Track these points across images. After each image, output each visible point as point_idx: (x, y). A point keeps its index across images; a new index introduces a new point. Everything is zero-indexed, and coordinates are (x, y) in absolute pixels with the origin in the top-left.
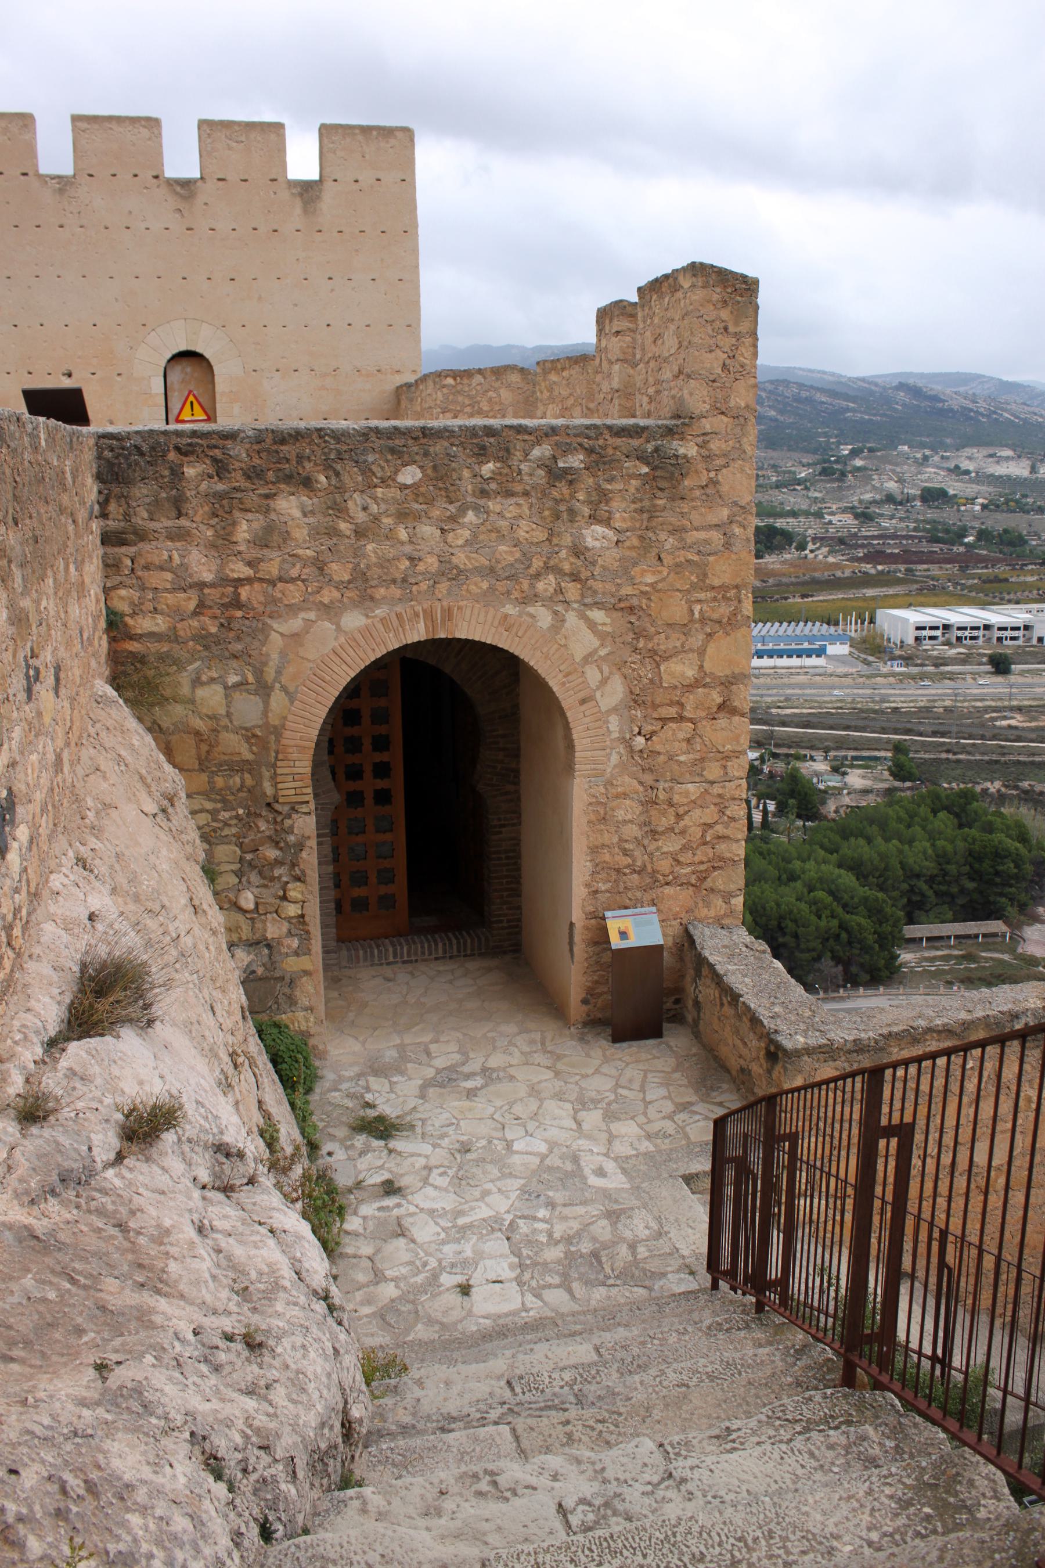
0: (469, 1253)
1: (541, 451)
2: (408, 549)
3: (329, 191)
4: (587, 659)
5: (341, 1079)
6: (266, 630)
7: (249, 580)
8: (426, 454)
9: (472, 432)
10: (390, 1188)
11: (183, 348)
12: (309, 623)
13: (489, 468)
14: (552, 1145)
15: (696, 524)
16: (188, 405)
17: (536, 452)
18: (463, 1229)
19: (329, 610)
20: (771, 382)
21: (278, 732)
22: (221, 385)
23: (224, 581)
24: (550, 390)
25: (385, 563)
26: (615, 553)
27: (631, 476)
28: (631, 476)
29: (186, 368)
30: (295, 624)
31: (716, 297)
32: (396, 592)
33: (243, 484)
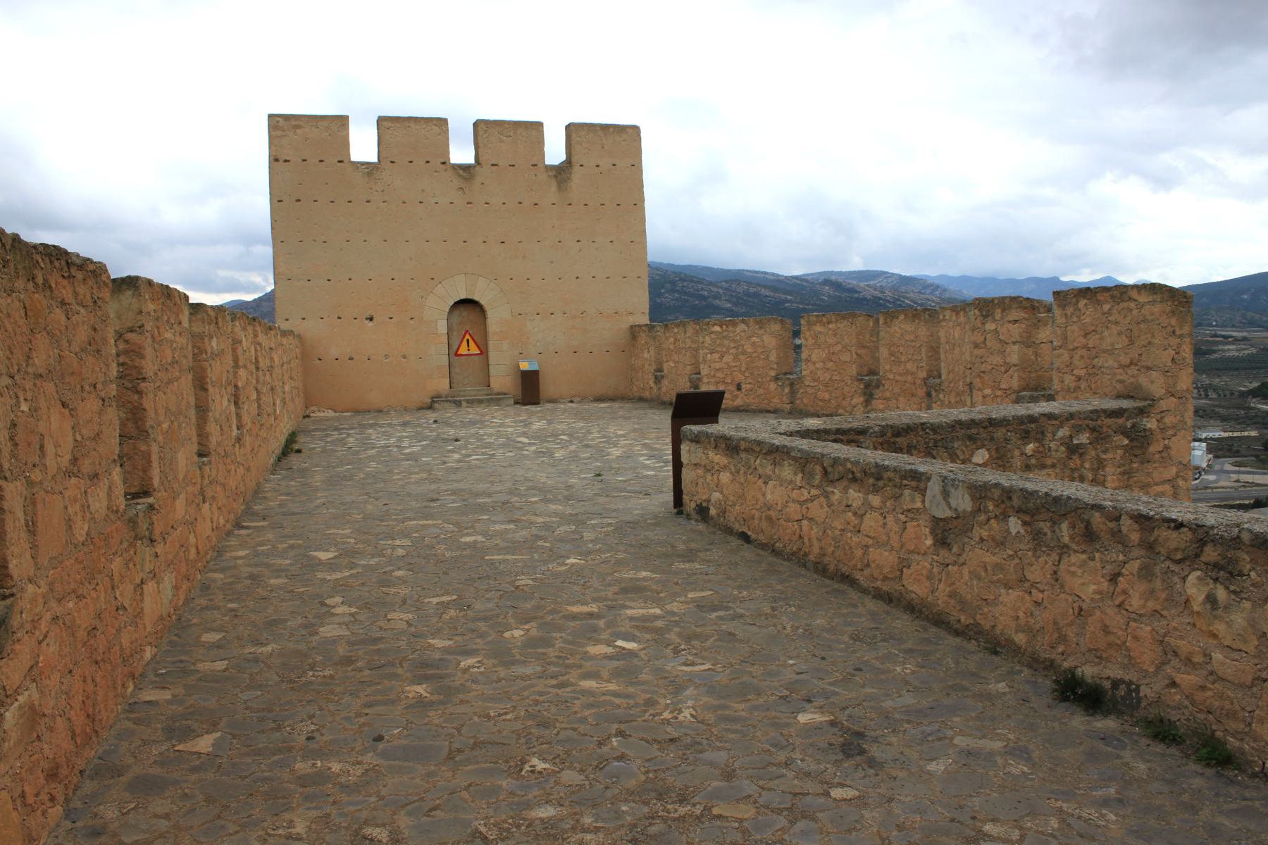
1: (1063, 432)
3: (577, 174)
8: (992, 439)
9: (1021, 420)
11: (463, 297)
13: (1030, 447)
15: (1156, 480)
16: (465, 342)
20: (726, 282)
24: (815, 337)
27: (1118, 447)
28: (1118, 447)
29: (465, 312)
31: (1168, 309)
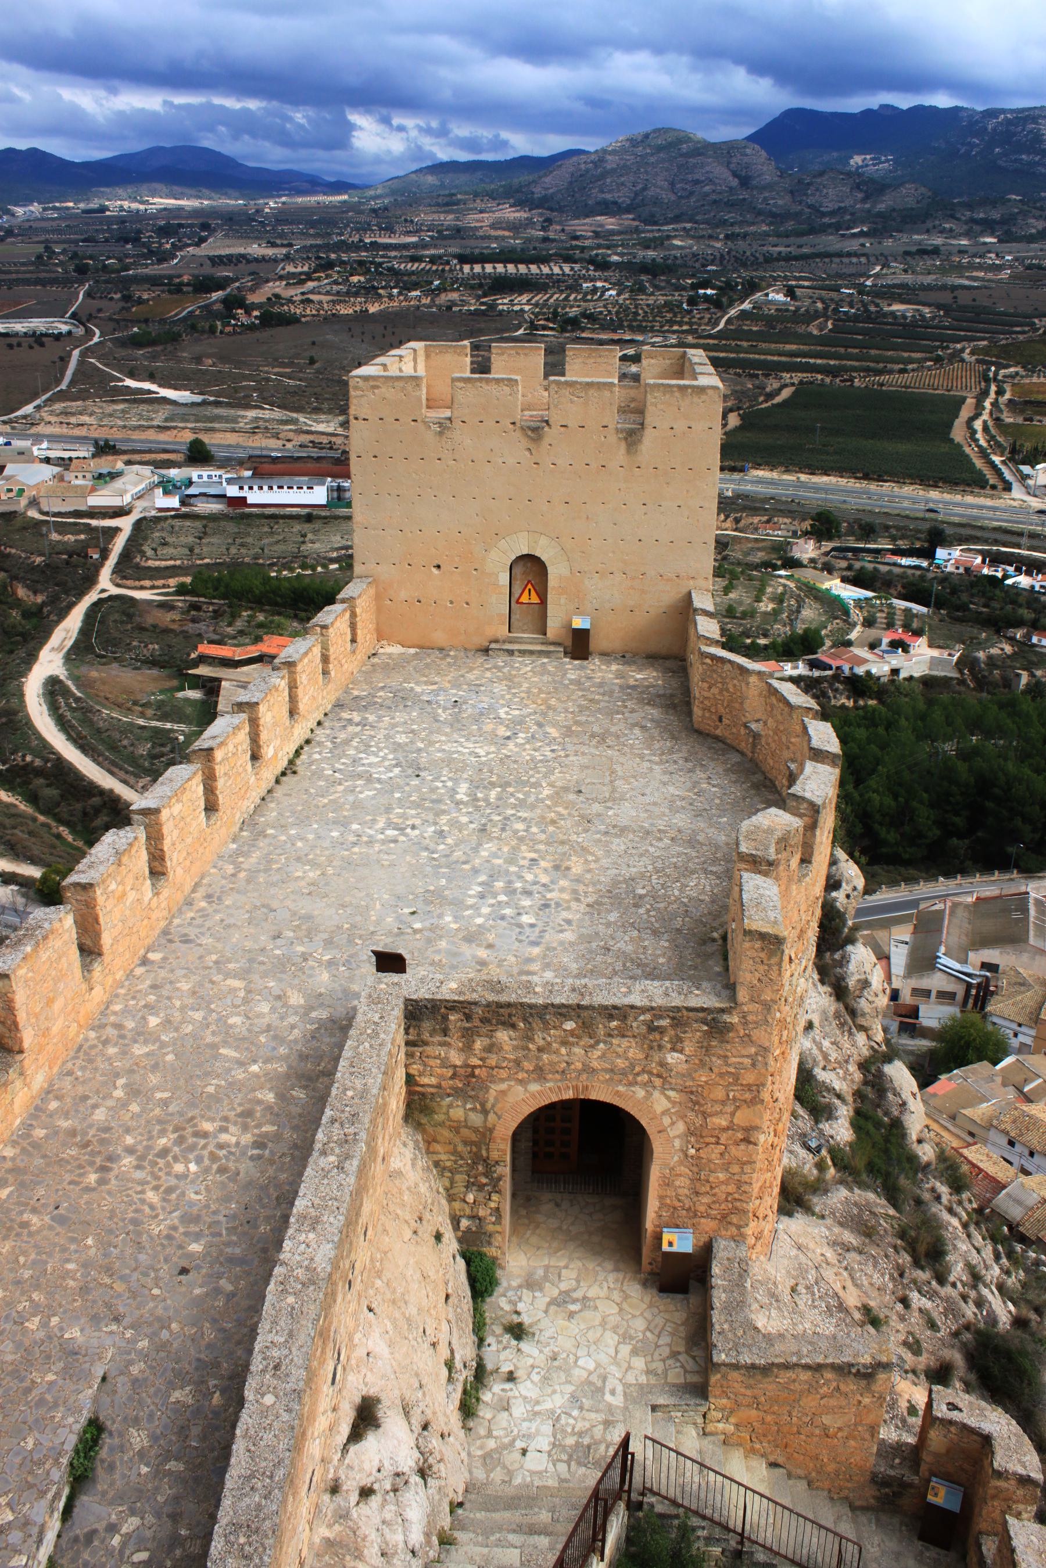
0: (533, 1430)
1: (648, 1017)
2: (566, 1058)
4: (663, 1113)
5: (507, 1289)
6: (487, 1089)
7: (480, 1066)
10: (511, 1377)
12: (510, 1087)
14: (598, 1365)
17: (642, 1018)
18: (536, 1414)
19: (521, 1082)
21: (491, 1130)
22: (552, 582)
23: (466, 1066)
25: (552, 1063)
26: (685, 1066)
30: (503, 1086)
32: (558, 1076)
33: (479, 1024)
